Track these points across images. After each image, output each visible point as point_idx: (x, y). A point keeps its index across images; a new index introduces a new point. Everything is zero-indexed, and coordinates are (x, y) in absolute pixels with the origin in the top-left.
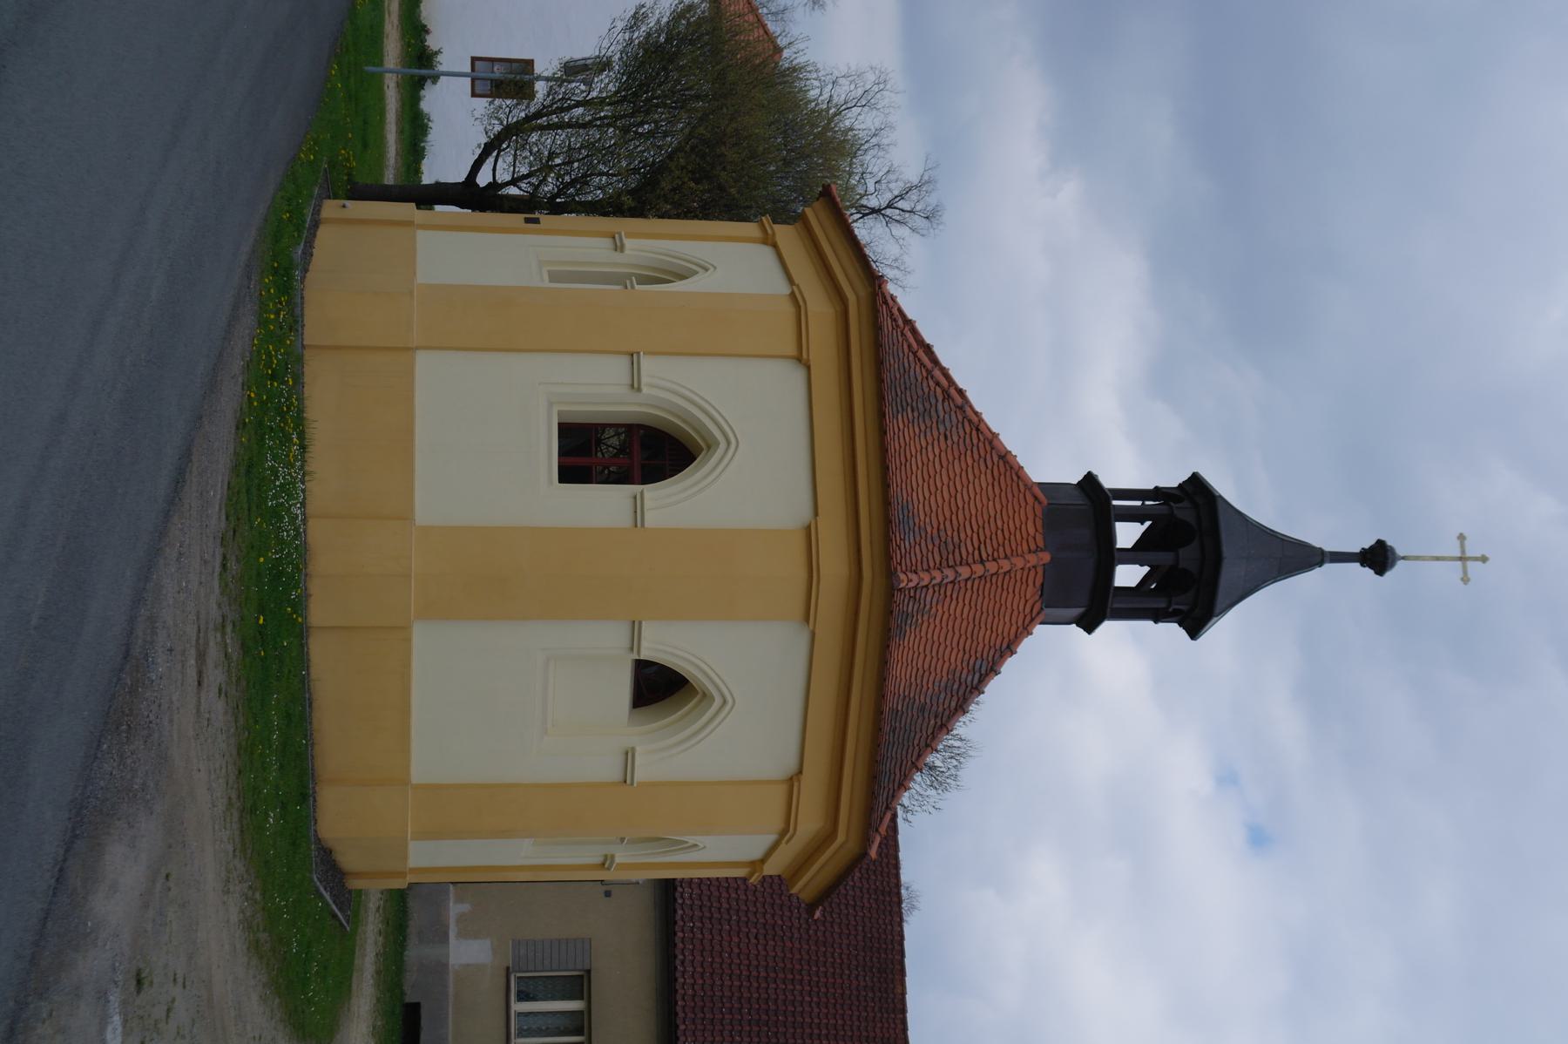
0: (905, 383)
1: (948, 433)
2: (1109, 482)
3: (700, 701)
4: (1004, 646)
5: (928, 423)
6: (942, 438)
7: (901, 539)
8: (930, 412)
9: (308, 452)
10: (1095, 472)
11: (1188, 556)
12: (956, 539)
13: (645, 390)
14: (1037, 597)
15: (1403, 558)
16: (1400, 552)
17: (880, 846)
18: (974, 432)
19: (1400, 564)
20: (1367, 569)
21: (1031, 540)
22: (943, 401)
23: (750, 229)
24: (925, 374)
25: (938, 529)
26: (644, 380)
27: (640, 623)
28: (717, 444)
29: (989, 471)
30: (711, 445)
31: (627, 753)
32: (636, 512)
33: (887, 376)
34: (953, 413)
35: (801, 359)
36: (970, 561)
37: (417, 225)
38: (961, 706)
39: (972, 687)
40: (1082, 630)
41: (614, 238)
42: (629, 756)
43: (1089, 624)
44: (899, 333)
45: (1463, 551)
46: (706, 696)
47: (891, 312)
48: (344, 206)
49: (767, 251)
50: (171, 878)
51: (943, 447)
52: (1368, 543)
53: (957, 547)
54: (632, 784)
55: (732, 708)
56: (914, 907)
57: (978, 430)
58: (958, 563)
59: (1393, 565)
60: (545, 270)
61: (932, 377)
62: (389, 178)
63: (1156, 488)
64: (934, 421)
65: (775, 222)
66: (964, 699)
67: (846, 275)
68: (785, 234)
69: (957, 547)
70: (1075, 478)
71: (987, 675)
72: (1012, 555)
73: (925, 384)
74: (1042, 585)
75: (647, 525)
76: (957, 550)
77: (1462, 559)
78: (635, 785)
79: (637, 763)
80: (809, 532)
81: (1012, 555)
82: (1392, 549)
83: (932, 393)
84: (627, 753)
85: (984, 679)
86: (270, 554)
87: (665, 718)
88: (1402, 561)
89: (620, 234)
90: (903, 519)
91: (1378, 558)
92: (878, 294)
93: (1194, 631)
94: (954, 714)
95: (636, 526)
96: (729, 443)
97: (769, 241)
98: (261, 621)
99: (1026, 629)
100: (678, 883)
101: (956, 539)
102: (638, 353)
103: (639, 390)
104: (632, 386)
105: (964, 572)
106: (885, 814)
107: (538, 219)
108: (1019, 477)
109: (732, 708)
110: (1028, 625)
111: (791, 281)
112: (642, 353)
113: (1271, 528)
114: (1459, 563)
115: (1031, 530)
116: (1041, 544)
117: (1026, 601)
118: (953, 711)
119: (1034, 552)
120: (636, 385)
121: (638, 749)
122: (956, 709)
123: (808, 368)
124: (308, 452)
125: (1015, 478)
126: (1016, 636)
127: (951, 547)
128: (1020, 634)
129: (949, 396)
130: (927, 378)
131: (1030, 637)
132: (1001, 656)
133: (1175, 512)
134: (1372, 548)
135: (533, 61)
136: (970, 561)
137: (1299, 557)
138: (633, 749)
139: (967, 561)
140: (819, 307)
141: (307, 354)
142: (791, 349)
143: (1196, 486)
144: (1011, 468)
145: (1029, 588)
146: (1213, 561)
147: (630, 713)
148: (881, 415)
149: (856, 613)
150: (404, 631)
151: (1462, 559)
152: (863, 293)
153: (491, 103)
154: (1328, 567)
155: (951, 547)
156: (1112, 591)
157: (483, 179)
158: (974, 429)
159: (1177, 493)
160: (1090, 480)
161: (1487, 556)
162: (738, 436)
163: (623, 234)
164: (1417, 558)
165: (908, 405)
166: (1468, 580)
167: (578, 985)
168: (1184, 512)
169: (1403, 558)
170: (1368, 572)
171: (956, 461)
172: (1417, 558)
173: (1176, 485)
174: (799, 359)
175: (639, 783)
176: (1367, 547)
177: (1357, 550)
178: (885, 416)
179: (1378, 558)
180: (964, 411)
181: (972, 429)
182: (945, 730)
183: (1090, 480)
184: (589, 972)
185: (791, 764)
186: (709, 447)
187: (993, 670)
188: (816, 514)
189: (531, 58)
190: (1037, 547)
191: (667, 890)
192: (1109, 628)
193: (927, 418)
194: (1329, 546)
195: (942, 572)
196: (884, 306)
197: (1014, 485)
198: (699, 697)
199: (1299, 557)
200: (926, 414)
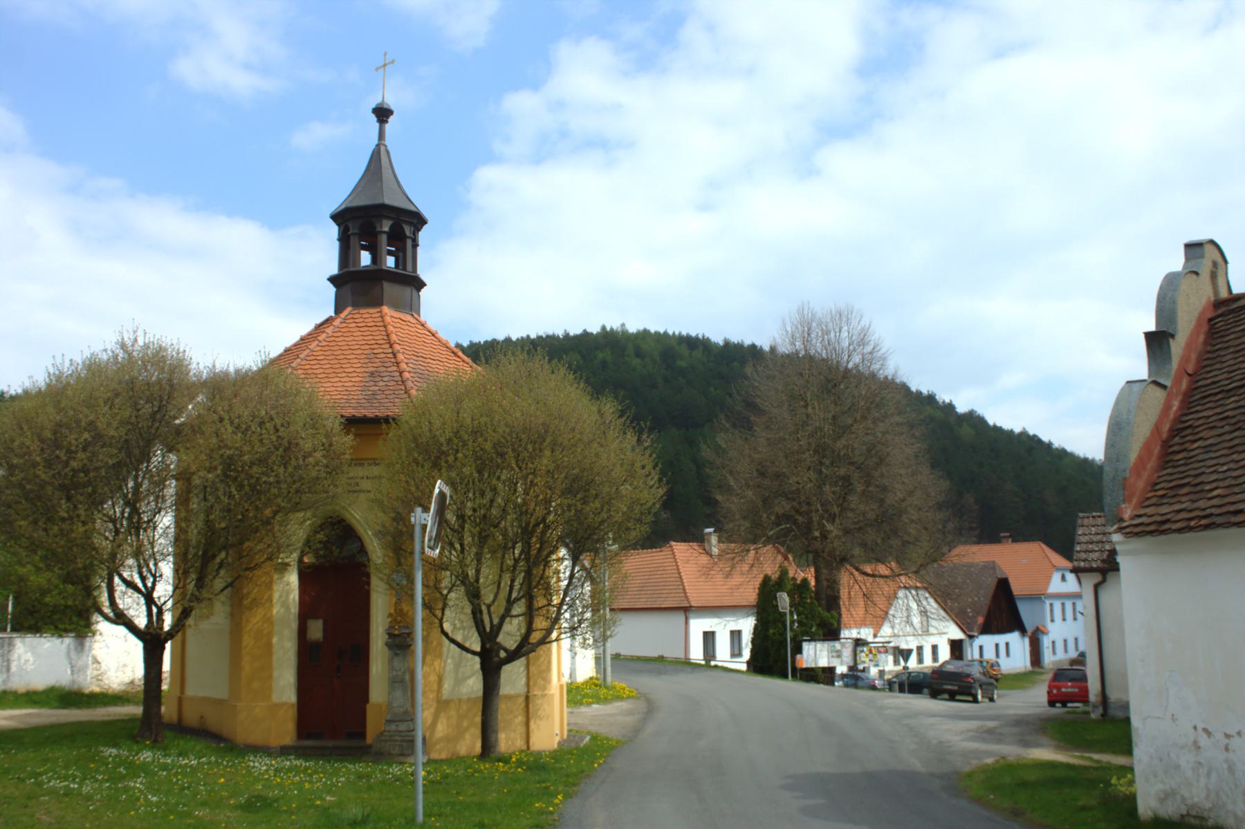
2: (334, 270)
16: (379, 100)
43: (419, 284)
52: (374, 118)
56: (842, 316)
86: (274, 782)
91: (382, 114)
107: (740, 655)
113: (357, 180)
135: (425, 285)
137: (377, 164)
146: (382, 210)
153: (62, 642)
159: (342, 228)
160: (333, 280)
177: (378, 125)
179: (382, 114)
189: (1143, 336)
192: (422, 273)
199: (377, 164)
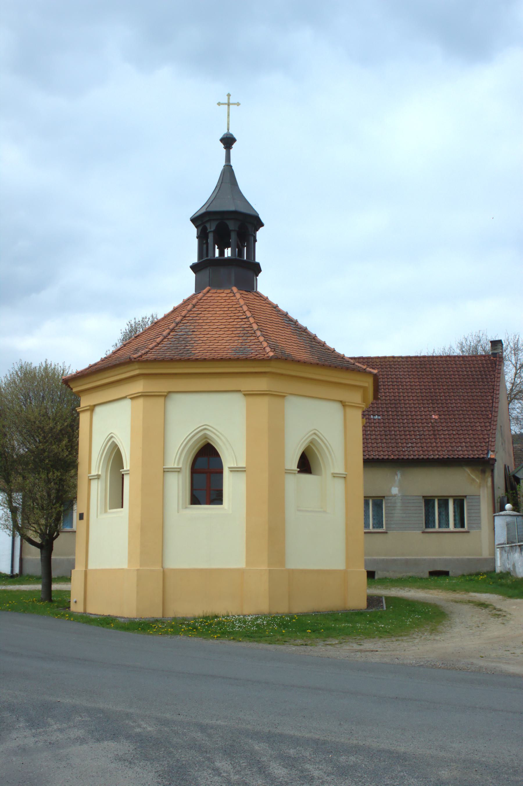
0: (175, 349)
1: (191, 330)
3: (314, 445)
4: (274, 309)
5: (189, 339)
6: (194, 333)
7: (252, 354)
8: (184, 338)
9: (218, 614)
10: (191, 264)
11: (232, 225)
12: (241, 329)
13: (180, 466)
14: (251, 294)
15: (228, 130)
16: (226, 131)
17: (373, 368)
18: (186, 318)
19: (231, 132)
20: (233, 146)
21: (229, 295)
22: (176, 332)
23: (84, 418)
24: (166, 340)
25: (239, 337)
26: (176, 466)
27: (286, 470)
28: (205, 434)
29: (203, 313)
30: (205, 437)
31: (334, 476)
32: (238, 471)
33: (178, 357)
34: (180, 328)
35: (166, 396)
36: (248, 323)
37: (85, 569)
38: (305, 330)
39: (295, 325)
40: (260, 274)
41: (91, 479)
42: (335, 476)
44: (152, 351)
45: (225, 104)
46: (312, 442)
47: (144, 354)
48: (76, 602)
49: (98, 410)
50: (482, 656)
51: (199, 333)
53: (244, 329)
54: (346, 475)
55: (317, 431)
57: (185, 317)
58: (252, 329)
59: (232, 135)
60: (109, 511)
61: (167, 336)
62: (39, 587)
63: (197, 238)
64: (187, 336)
65: (80, 406)
66: (301, 328)
67: (117, 375)
68: (85, 402)
69: (244, 329)
70: (192, 275)
71: (288, 318)
72: (239, 304)
73: (171, 340)
74: (246, 291)
75: (244, 466)
76: (246, 329)
77: (229, 104)
78: (346, 473)
79: (338, 472)
80: (247, 395)
81: (239, 304)
82: (224, 135)
83: (174, 337)
84: (334, 476)
85: (291, 319)
87: (318, 458)
88: (229, 131)
89: (89, 477)
90: (169, 353)
92: (139, 360)
93: (262, 225)
94: (308, 333)
95: (245, 471)
96: (205, 429)
97: (92, 409)
98: (310, 631)
99: (266, 299)
100: (366, 458)
101: (241, 329)
102: (164, 468)
103: (180, 468)
104: (179, 471)
105: (255, 327)
106: (356, 365)
108: (201, 299)
109: (317, 431)
110: (264, 299)
111: (125, 398)
112: (164, 467)
114: (231, 106)
115: (224, 295)
116: (229, 291)
117: (255, 299)
118: (307, 334)
119: (235, 294)
120: (179, 470)
121: (332, 471)
122: (306, 332)
123: (170, 392)
124: (218, 614)
125: (202, 301)
126: (270, 304)
127: (245, 332)
128: (268, 302)
129: (173, 329)
130: (168, 339)
131: (268, 298)
132: (279, 311)
133: (212, 230)
134: (224, 144)
136: (248, 323)
138: (332, 474)
139: (249, 325)
140: (138, 387)
141: (170, 614)
142: (162, 400)
143: (196, 220)
144: (198, 302)
145: (250, 297)
146: (235, 215)
147: (314, 474)
148: (189, 360)
149: (282, 375)
150: (292, 572)
151: (229, 104)
152: (136, 366)
154: (232, 163)
155: (245, 332)
156: (247, 260)
157: (38, 540)
158: (184, 319)
159: (200, 228)
160: (194, 268)
161: (227, 94)
162: (202, 425)
163: (89, 475)
164: (228, 124)
165: (185, 348)
166: (238, 103)
167: (428, 502)
168: (211, 227)
169: (228, 130)
170: (234, 146)
171: (203, 327)
172: (228, 124)
173: (196, 229)
174: (165, 396)
175: (345, 472)
176: (223, 146)
178: (198, 359)
180: (178, 322)
181: (185, 319)
182: (315, 338)
183: (194, 268)
184: (423, 497)
185: (337, 407)
186: (206, 438)
187: (286, 315)
188: (239, 391)
190: (231, 292)
191: (369, 462)
193: (187, 340)
194: (223, 163)
195: (259, 336)
196: (143, 357)
197: (205, 301)
198: (311, 445)
200: (186, 340)
